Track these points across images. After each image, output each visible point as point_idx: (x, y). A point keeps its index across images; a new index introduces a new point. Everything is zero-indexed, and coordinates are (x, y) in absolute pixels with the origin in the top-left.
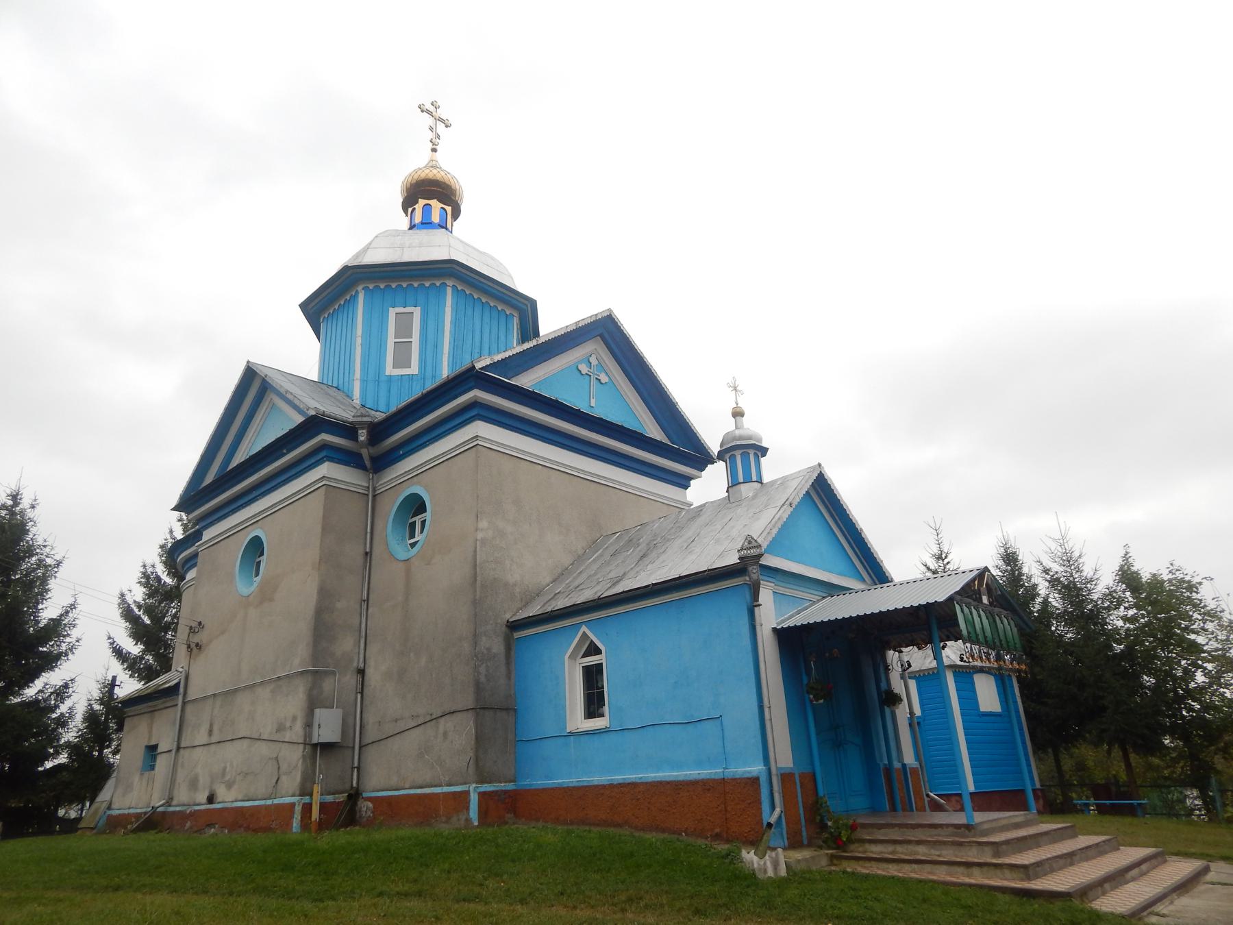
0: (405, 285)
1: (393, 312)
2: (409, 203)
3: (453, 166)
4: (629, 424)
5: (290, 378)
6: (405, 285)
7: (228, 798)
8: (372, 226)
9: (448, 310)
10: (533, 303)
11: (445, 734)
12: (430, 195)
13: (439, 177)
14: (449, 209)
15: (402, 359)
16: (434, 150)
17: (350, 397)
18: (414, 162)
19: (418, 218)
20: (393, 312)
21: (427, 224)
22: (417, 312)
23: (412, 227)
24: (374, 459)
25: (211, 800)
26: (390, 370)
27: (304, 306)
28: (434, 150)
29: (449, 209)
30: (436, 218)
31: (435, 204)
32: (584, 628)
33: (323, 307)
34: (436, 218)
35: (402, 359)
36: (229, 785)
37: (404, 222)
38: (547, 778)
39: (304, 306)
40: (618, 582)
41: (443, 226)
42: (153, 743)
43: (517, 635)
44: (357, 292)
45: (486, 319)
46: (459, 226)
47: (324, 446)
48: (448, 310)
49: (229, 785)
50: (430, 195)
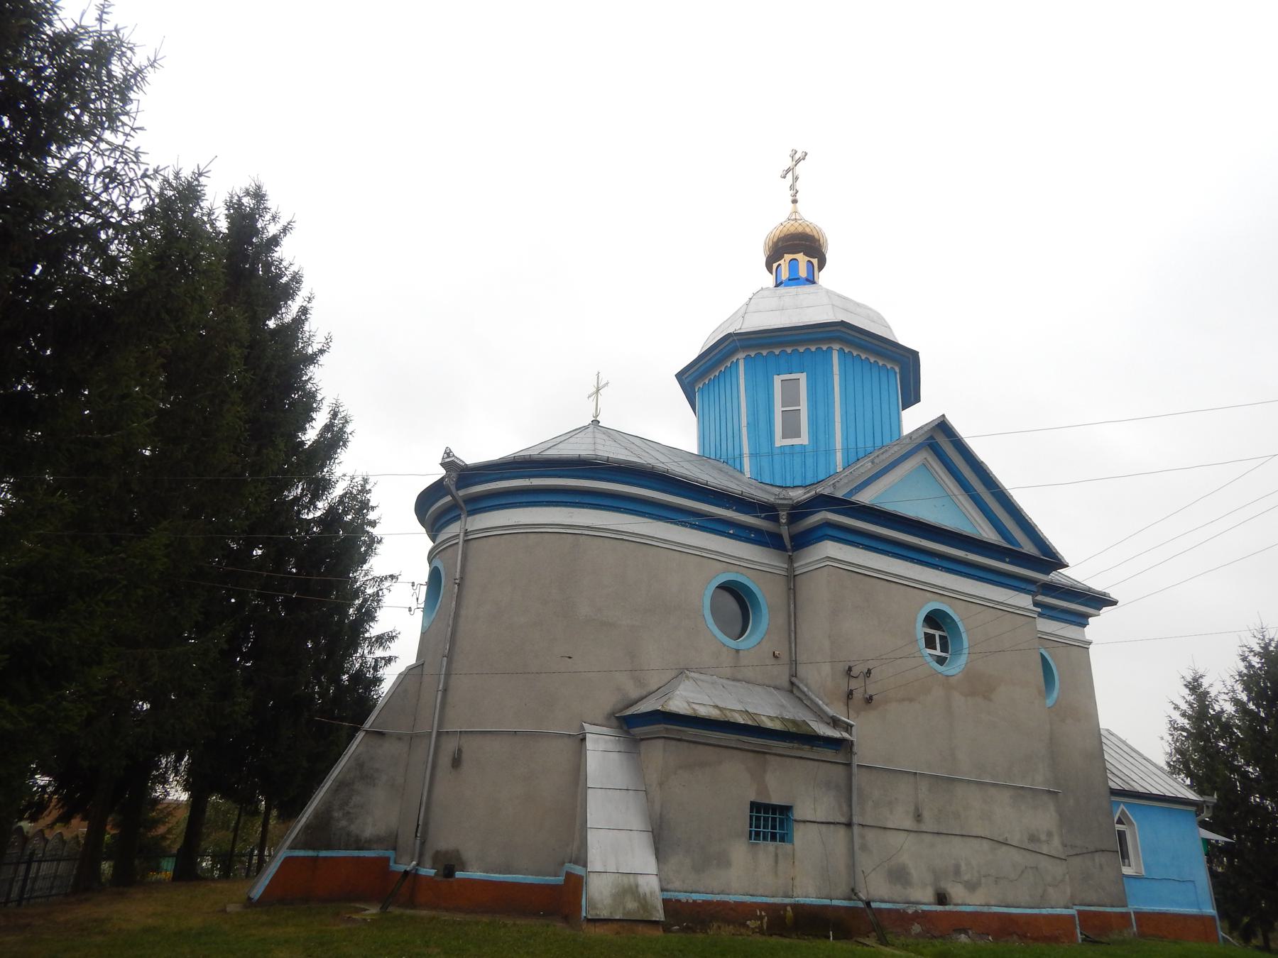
0: (813, 349)
1: (777, 380)
2: (773, 258)
3: (814, 216)
4: (967, 530)
5: (637, 442)
6: (813, 349)
7: (966, 900)
8: (738, 292)
9: (836, 379)
10: (914, 355)
11: (1101, 866)
12: (797, 250)
13: (800, 230)
14: (815, 261)
15: (791, 429)
16: (795, 201)
17: (741, 472)
18: (773, 219)
19: (785, 275)
20: (777, 380)
21: (794, 280)
22: (803, 377)
23: (778, 284)
24: (793, 538)
25: (942, 898)
26: (779, 442)
27: (680, 376)
28: (795, 201)
29: (815, 261)
30: (803, 273)
31: (802, 258)
32: (1122, 806)
33: (699, 378)
34: (803, 273)
35: (791, 429)
36: (972, 887)
37: (769, 280)
38: (329, 848)
39: (680, 376)
40: (631, 705)
41: (811, 281)
42: (776, 800)
43: (1114, 798)
44: (830, 349)
45: (884, 386)
46: (824, 277)
47: (829, 524)
48: (836, 379)
49: (972, 887)
50: (797, 250)
